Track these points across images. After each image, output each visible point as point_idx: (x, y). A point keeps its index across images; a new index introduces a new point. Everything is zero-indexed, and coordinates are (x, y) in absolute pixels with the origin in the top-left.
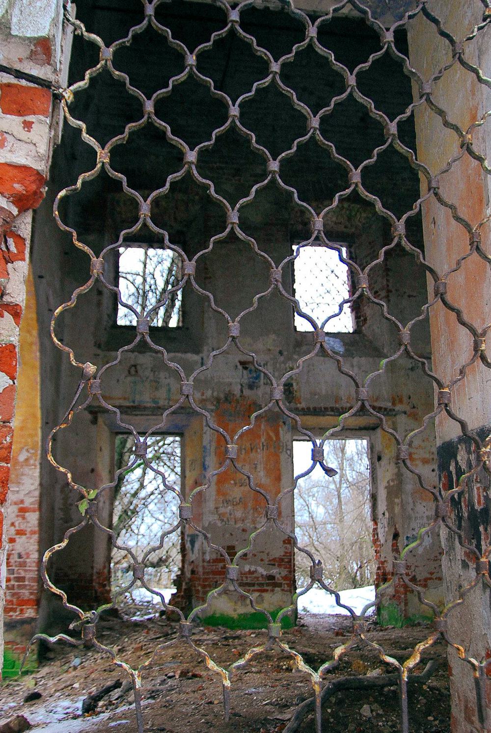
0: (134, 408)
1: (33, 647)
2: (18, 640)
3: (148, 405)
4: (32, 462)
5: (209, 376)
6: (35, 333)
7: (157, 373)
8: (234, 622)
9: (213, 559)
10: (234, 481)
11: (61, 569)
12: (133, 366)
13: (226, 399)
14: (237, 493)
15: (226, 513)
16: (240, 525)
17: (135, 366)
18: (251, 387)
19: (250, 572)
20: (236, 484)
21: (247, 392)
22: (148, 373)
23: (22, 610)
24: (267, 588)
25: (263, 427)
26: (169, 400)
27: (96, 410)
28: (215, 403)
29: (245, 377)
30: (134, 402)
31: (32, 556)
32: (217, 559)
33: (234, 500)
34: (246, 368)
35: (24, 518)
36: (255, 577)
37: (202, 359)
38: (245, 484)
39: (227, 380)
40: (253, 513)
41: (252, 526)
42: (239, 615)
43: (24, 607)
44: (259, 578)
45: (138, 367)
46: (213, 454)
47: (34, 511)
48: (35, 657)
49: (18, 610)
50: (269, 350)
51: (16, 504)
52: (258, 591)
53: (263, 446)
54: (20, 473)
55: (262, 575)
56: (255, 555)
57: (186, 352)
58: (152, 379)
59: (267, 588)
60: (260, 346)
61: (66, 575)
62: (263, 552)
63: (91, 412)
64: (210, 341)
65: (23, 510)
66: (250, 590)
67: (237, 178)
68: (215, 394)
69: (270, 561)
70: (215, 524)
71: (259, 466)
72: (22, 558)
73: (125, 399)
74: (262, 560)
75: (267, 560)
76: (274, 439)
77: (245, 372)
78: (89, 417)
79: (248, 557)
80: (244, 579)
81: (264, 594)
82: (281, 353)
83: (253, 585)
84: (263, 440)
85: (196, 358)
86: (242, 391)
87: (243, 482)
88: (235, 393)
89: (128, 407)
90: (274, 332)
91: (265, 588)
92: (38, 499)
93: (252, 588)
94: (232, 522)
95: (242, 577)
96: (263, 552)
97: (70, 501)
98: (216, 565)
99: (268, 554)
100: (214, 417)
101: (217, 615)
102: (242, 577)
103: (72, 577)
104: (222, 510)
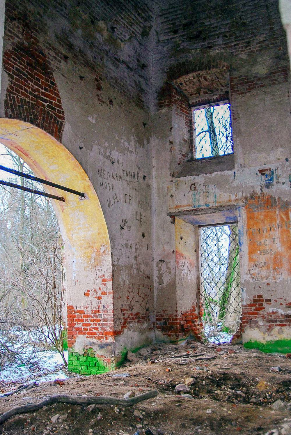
0: (196, 210)
1: (113, 359)
2: (106, 355)
3: (203, 208)
4: (107, 252)
5: (239, 183)
6: (88, 179)
7: (207, 186)
8: (263, 346)
9: (248, 304)
10: (259, 251)
11: (159, 313)
12: (193, 184)
13: (252, 197)
14: (262, 259)
15: (256, 273)
16: (265, 281)
17: (194, 184)
18: (267, 186)
19: (273, 313)
20: (261, 253)
21: (265, 190)
22: (202, 187)
23: (106, 338)
24: (286, 323)
25: (277, 213)
26: (215, 202)
27: (174, 214)
28: (244, 201)
29: (263, 180)
30: (195, 207)
31: (110, 307)
32: (251, 304)
33: (261, 264)
34: (263, 174)
35: (105, 285)
36: (277, 316)
37: (234, 173)
38: (267, 253)
39: (251, 184)
40: (274, 272)
41: (273, 281)
42: (267, 342)
43: (107, 336)
44: (279, 316)
45: (196, 185)
46: (245, 234)
47: (110, 281)
48: (114, 365)
49: (105, 337)
50: (279, 159)
51: (100, 277)
52: (280, 325)
53: (278, 225)
54: (102, 259)
55: (282, 315)
56: (276, 301)
57: (224, 170)
58: (205, 191)
59: (286, 323)
60: (272, 157)
61: (162, 316)
62: (282, 299)
63: (171, 217)
64: (238, 161)
65: (104, 280)
66: (273, 325)
67: (248, 48)
68: (244, 195)
69: (287, 304)
70: (249, 281)
71: (276, 240)
72: (105, 308)
73: (189, 206)
74: (281, 304)
75: (285, 304)
76: (285, 219)
77: (263, 176)
78: (169, 219)
79: (272, 302)
80: (269, 317)
81: (283, 328)
82: (287, 160)
83: (276, 321)
84: (278, 222)
85: (231, 173)
86: (262, 190)
87: (266, 251)
88: (257, 192)
89: (192, 211)
90: (282, 146)
91: (284, 323)
92: (111, 273)
93: (275, 324)
94: (260, 279)
95: (268, 316)
96: (282, 299)
97: (162, 272)
98: (250, 308)
99: (285, 300)
100: (244, 210)
101: (253, 342)
102: (268, 316)
103: (165, 317)
104: (253, 272)
